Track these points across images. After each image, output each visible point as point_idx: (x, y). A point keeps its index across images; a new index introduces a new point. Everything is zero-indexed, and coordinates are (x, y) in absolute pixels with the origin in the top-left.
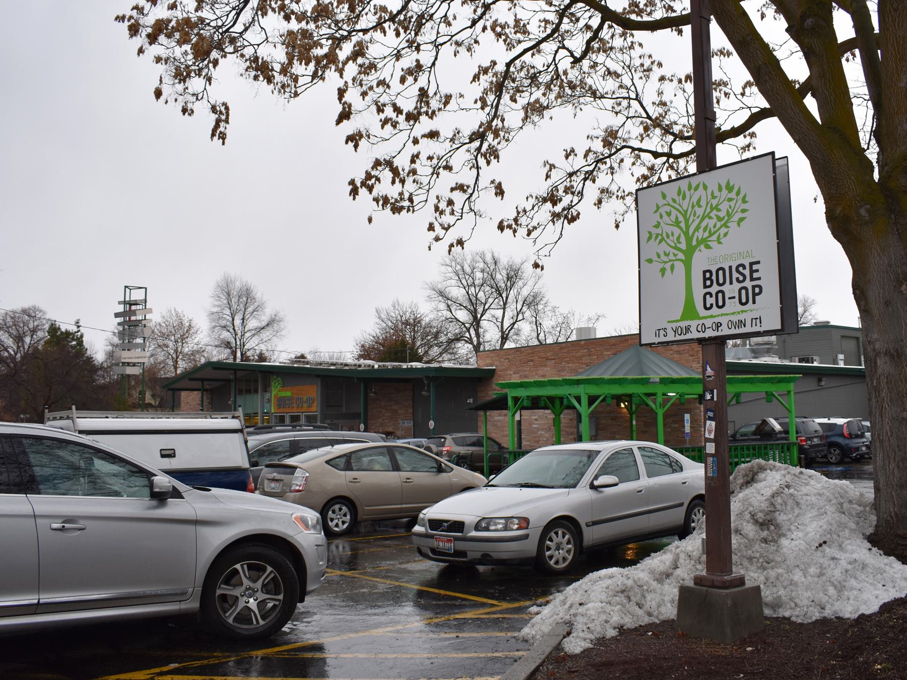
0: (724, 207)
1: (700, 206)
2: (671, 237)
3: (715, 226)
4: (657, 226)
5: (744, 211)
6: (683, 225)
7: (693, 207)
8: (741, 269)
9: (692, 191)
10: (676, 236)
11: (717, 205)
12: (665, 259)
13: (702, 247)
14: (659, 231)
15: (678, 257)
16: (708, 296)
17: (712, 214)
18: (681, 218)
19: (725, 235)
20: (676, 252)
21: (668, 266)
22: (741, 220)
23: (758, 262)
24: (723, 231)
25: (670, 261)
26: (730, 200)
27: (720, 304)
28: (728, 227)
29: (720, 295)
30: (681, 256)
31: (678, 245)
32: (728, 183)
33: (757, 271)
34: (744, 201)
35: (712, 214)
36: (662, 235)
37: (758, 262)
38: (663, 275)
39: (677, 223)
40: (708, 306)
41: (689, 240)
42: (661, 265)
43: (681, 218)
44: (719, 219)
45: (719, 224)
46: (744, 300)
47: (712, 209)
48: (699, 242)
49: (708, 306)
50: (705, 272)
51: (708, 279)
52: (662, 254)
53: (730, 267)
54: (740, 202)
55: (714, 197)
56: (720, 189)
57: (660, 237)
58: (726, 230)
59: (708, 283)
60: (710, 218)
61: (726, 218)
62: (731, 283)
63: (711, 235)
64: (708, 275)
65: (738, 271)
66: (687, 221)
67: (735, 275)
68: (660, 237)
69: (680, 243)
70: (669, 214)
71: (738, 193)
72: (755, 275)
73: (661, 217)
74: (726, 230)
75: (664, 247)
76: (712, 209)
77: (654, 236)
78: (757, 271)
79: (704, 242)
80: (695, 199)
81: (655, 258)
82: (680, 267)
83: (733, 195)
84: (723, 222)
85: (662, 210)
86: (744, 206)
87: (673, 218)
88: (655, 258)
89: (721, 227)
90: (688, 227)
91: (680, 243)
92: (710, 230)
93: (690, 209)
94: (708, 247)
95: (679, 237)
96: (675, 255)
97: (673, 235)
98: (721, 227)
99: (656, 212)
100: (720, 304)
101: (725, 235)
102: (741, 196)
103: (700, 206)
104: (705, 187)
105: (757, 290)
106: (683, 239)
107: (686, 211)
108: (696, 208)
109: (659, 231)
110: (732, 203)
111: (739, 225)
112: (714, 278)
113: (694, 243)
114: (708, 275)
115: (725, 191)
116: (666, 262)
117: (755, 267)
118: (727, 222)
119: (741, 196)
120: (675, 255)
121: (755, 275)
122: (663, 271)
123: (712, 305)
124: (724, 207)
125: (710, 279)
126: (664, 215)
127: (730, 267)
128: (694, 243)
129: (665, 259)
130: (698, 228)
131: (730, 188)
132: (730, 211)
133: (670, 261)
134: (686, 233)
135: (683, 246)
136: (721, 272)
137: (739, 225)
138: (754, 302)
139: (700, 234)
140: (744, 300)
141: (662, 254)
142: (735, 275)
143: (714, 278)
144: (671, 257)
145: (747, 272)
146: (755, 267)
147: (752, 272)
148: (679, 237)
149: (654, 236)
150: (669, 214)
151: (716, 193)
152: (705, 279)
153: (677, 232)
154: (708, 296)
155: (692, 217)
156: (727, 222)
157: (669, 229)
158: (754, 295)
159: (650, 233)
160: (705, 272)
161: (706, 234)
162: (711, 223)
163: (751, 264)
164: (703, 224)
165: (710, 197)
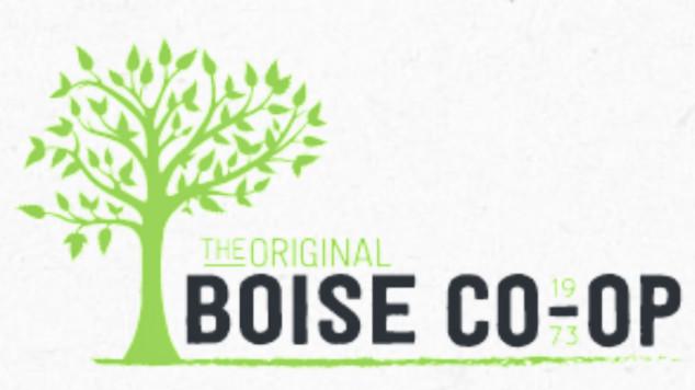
0: (260, 123)
1: (192, 107)
2: (103, 165)
3: (232, 161)
4: (64, 129)
5: (311, 141)
6: (141, 141)
7: (172, 104)
8: (340, 293)
9: (172, 67)
10: (118, 164)
11: (243, 114)
12: (86, 214)
13: (194, 203)
14: (67, 143)
15: (122, 216)
16: (468, 293)
17: (225, 133)
18: (135, 124)
19: (260, 186)
20: (118, 203)
21: (92, 233)
22: (301, 163)
23: (407, 281)
24: (254, 176)
25: (98, 220)
26: (276, 110)
27: (518, 325)
28: (268, 170)
29: (517, 295)
30: (133, 214)
31: (125, 188)
32: (273, 70)
33: (402, 309)
34: (314, 117)
35: (225, 133)
36: (75, 154)
37: (407, 281)
38: (75, 251)
39: (123, 134)
40: (468, 327)
41: (157, 180)
42: (73, 228)
43: (135, 124)
44: (244, 147)
45: (243, 160)
46: (609, 325)
47: (226, 120)
48: (186, 192)
49: (468, 327)
50: (195, 284)
51: (208, 310)
52: (75, 203)
53: (300, 283)
54: (303, 119)
55: (231, 93)
56: (251, 78)
57: (69, 160)
58: (263, 176)
59: (208, 324)
60: (221, 140)
61: (264, 149)
62: (300, 337)
63: (220, 178)
64: (207, 295)
65: (327, 297)
66: (153, 135)
67: (317, 311)
68: (69, 160)
69: (130, 183)
70: (100, 108)
71: (300, 97)
72: (394, 323)
73: (76, 109)
74: (263, 176)
75: (77, 185)
76: (226, 120)
77: (50, 155)
78: (402, 309)
79: (202, 193)
80: (178, 88)
81: (51, 206)
82: (127, 243)
83: (285, 100)
84: (254, 157)
85: (82, 95)
86: (312, 131)
87: (113, 121)
88: (51, 206)
89: (250, 166)
90: (155, 148)
91: (130, 183)
92: (219, 168)
93: (163, 110)
94: (212, 207)
95: (126, 172)
96: (112, 209)
97: (109, 159)
98: (250, 166)
99: (57, 95)
100: (518, 325)
101: (260, 186)
102: (307, 106)
103: (192, 107)
104: (210, 66)
105: (660, 296)
106: (138, 173)
107: (152, 112)
108: (182, 110)
109: (67, 143)
110: (283, 120)
111: (297, 171)
112: (233, 307)
113: (172, 189)
114: (207, 295)
115: (263, 90)
116: (84, 223)
117: (394, 295)
118: (267, 157)
119: (307, 106)
120: (112, 209)
121: (394, 323)
122: (76, 243)
123: (482, 328)
124: (260, 123)
125: (217, 309)
126: (86, 109)
127: (300, 283)
128: (172, 189)
129: (86, 214)
130: (183, 158)
131: (277, 83)
132: (276, 136)
133: (98, 220)
134: (150, 164)
135: (140, 190)
136: (260, 295)
137: (297, 171)
138: (647, 338)
139: (190, 173)
140: (609, 325)
141: (75, 203)
142: (317, 311)
143: (233, 307)
144: (103, 212)
145: (363, 308)
146: (394, 295)
147: (382, 310)
148: (126, 172)
149: (50, 155)
150: (100, 108)
151: (240, 86)
152: (195, 310)
153: (122, 155)
154: (468, 293)
155: (167, 131)
156: (267, 157)
157: (100, 146)
158: (650, 313)
159: (37, 142)
160: (195, 284)
161: (207, 176)
162: (223, 154)
163: (381, 284)
164: (201, 152)
165: (221, 92)
